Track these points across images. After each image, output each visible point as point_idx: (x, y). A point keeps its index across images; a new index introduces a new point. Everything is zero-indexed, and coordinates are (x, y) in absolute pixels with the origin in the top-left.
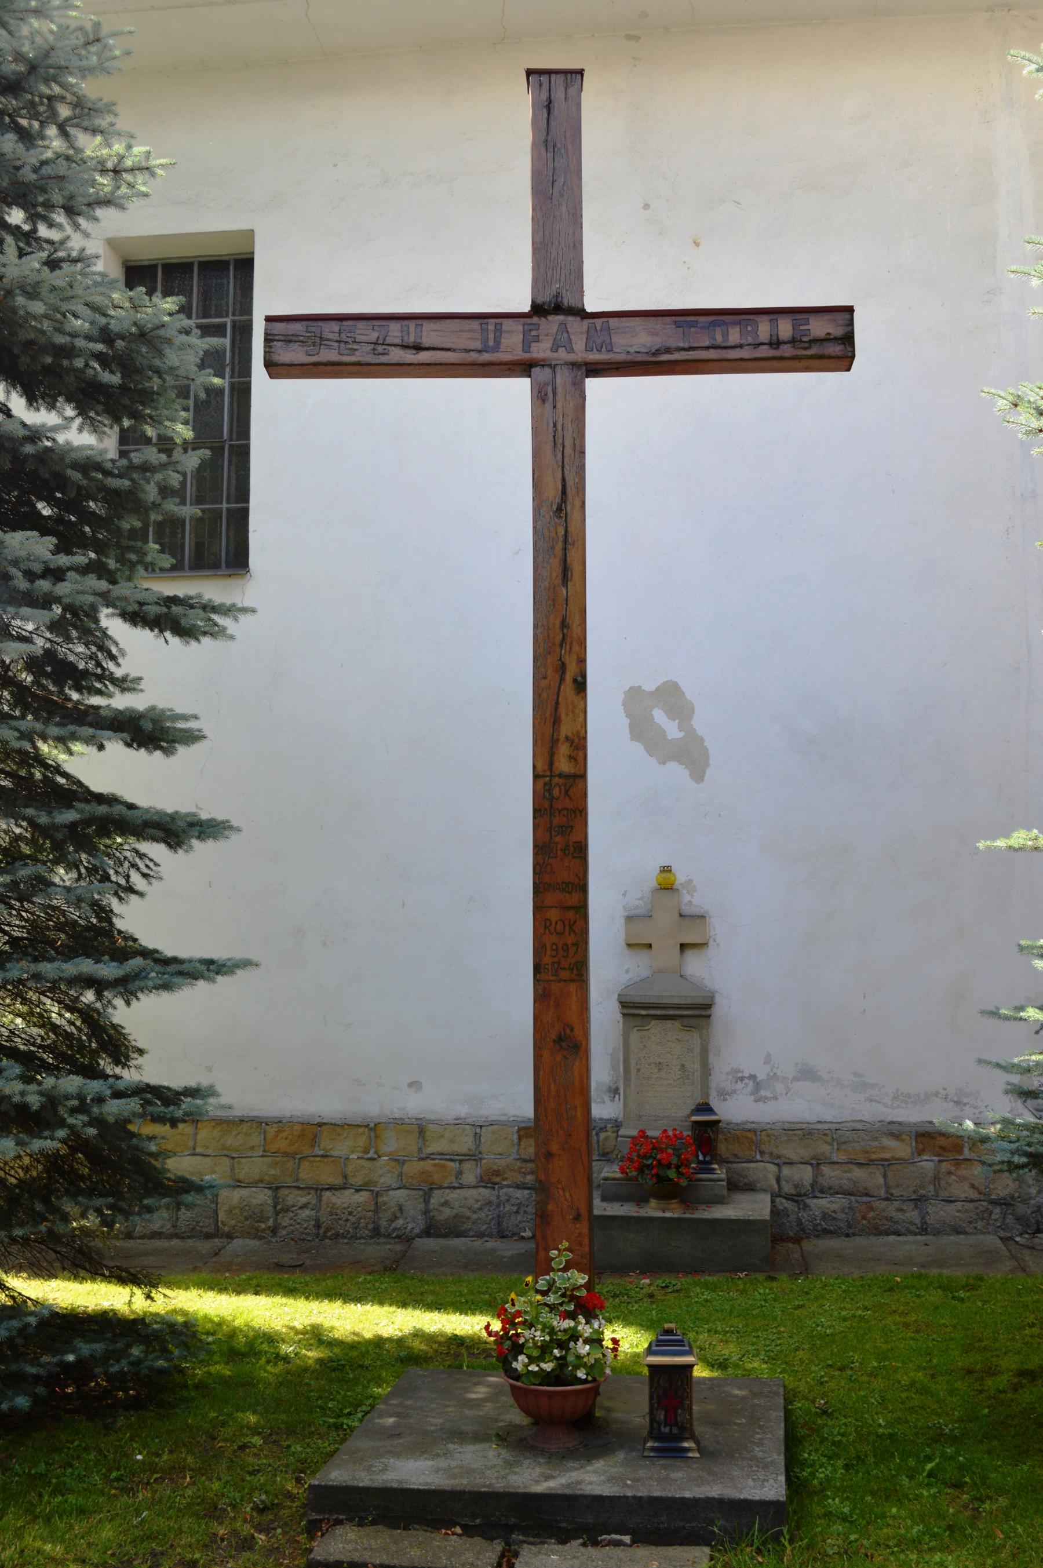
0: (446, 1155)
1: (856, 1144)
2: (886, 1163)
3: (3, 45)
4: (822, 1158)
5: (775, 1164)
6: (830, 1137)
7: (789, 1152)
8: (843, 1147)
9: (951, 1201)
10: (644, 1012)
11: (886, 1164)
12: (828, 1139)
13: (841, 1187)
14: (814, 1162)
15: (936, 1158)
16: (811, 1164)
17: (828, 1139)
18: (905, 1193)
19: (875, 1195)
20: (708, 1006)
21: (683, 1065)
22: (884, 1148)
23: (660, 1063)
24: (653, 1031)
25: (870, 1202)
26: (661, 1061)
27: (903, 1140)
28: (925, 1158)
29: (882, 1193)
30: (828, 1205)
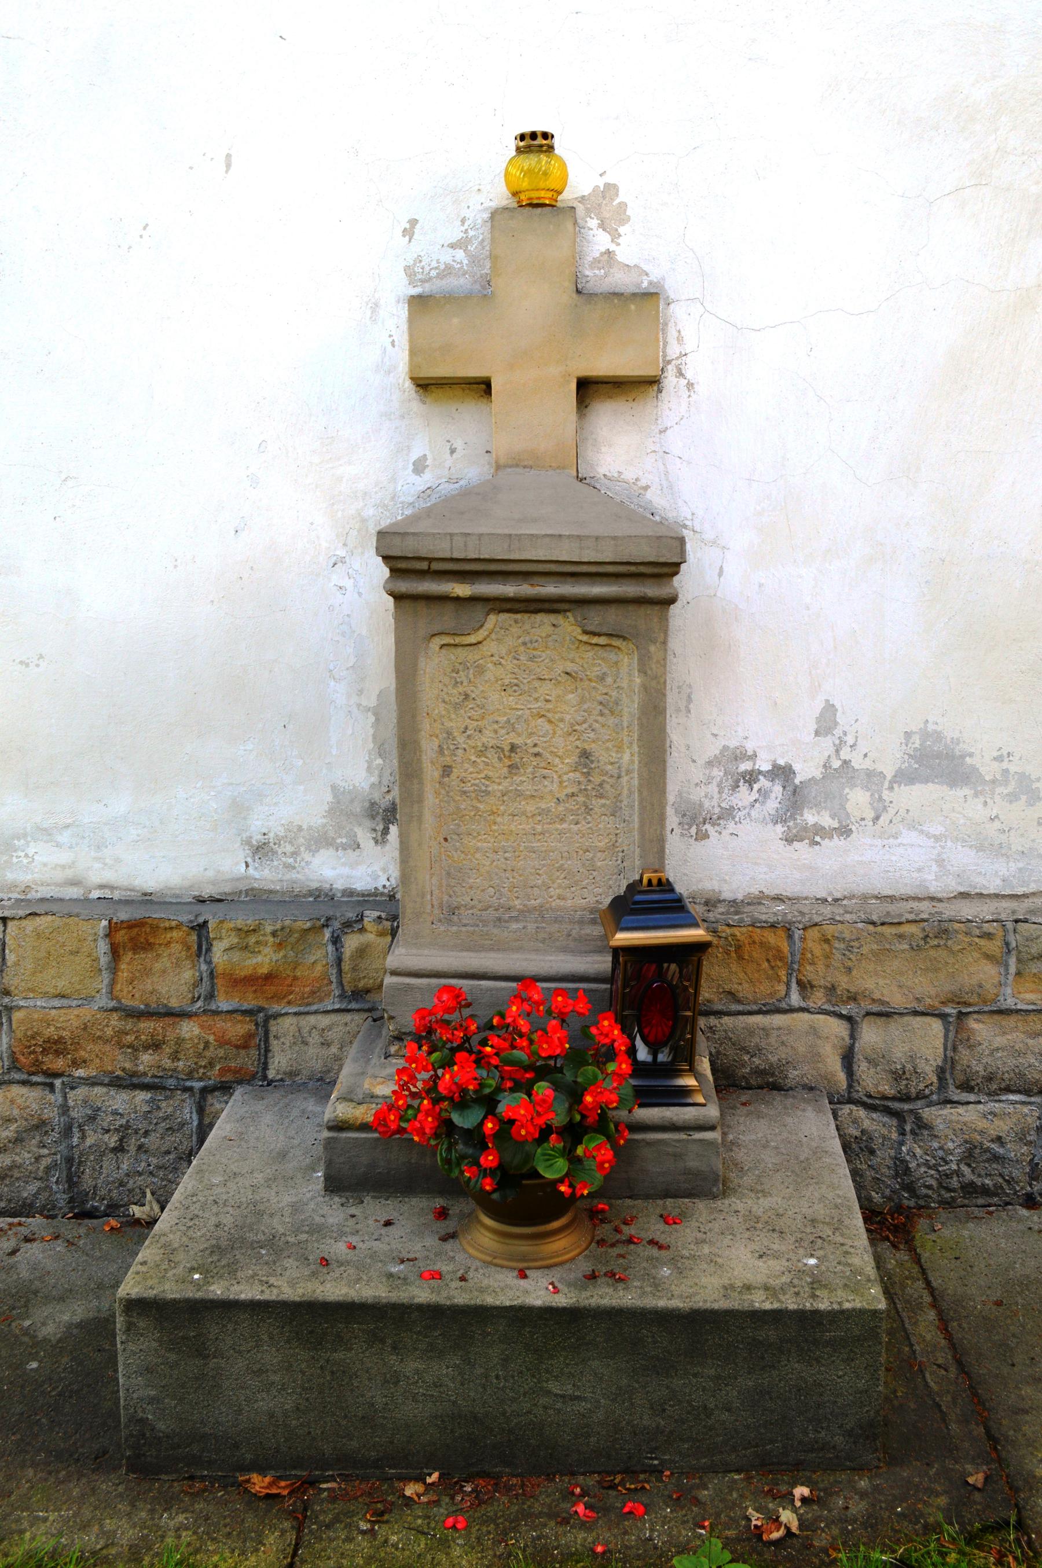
0: (473, 599)
4: (974, 999)
5: (840, 1016)
6: (998, 943)
10: (462, 590)
12: (994, 947)
16: (943, 1016)
20: (673, 568)
23: (513, 748)
26: (518, 741)
30: (982, 1124)
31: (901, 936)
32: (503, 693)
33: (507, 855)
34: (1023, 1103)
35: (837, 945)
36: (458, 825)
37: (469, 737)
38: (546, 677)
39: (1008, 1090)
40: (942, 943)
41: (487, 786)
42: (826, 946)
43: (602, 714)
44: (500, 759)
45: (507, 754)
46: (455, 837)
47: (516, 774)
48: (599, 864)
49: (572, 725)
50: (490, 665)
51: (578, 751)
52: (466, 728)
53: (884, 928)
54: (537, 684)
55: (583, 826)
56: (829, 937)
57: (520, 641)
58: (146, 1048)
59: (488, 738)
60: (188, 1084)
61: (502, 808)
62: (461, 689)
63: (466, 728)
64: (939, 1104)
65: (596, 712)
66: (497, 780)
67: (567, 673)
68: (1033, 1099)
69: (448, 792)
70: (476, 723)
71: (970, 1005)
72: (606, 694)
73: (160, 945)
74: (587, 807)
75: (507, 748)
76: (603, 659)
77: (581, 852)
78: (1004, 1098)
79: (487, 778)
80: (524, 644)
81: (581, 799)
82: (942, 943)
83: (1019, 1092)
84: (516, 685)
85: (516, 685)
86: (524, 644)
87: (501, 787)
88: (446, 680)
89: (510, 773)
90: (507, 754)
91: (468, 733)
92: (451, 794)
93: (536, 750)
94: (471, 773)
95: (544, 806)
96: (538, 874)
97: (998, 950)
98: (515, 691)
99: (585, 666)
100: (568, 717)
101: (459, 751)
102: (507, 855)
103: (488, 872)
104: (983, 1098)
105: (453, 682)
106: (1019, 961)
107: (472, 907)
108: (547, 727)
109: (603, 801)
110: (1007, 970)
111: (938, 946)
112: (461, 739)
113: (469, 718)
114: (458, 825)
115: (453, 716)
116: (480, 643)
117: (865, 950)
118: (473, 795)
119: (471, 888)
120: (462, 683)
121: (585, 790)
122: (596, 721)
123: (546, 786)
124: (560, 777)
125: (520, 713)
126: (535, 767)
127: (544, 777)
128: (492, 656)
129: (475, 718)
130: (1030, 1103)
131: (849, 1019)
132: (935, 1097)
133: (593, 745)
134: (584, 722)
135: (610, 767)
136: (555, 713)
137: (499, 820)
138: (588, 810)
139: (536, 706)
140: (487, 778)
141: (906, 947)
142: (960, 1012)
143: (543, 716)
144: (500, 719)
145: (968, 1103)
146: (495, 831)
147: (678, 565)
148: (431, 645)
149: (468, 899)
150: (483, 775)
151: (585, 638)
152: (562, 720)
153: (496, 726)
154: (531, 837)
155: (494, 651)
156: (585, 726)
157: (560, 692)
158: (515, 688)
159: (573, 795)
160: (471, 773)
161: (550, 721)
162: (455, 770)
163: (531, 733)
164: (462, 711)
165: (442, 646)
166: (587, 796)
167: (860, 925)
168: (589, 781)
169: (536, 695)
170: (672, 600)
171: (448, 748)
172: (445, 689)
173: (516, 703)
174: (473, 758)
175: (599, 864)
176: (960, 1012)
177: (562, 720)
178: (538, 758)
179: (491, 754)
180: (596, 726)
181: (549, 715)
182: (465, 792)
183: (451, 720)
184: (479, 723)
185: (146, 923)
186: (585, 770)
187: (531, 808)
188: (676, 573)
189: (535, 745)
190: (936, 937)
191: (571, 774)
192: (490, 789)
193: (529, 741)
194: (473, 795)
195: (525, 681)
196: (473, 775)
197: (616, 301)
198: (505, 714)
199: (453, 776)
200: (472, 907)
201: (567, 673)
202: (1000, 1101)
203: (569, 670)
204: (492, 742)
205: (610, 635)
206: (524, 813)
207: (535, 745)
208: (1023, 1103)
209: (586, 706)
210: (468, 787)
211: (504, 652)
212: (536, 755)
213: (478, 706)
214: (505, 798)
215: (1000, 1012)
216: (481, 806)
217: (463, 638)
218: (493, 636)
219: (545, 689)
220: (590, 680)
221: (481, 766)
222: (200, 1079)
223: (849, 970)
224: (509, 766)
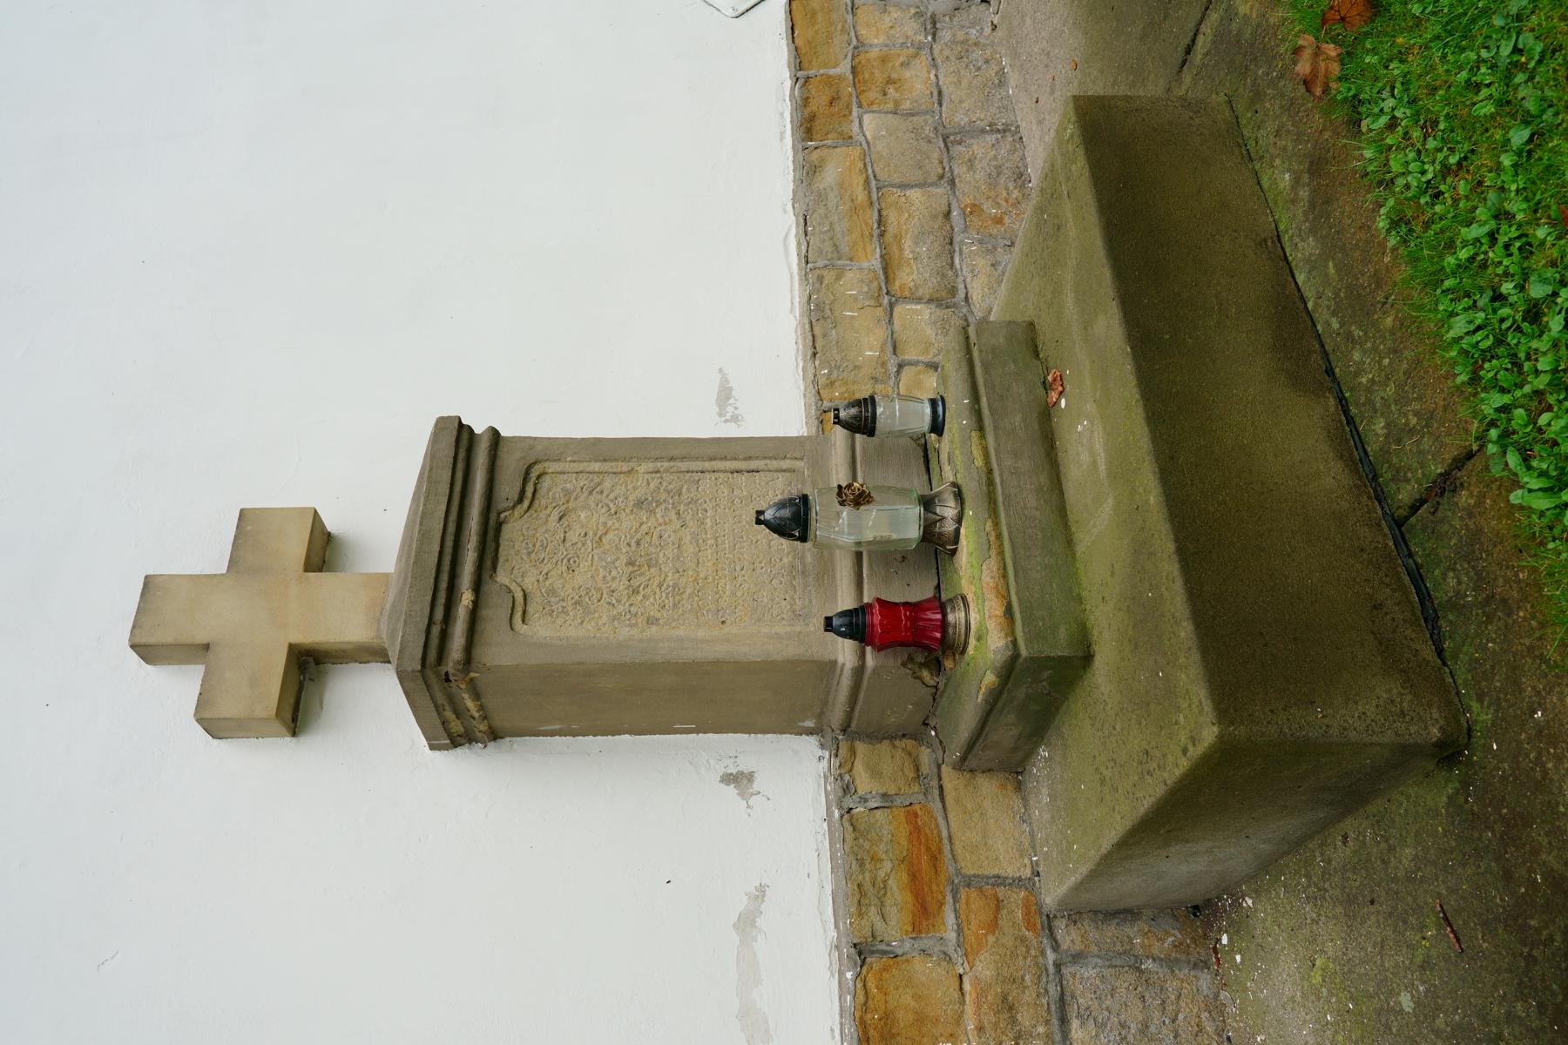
0: (477, 587)
1: (837, 228)
2: (873, 182)
3: (978, 1044)
4: (875, 285)
5: (898, 372)
6: (825, 273)
7: (869, 347)
8: (845, 249)
9: (940, 93)
10: (467, 598)
11: (876, 187)
12: (829, 276)
13: (938, 256)
14: (886, 301)
15: (855, 111)
16: (892, 306)
17: (829, 276)
18: (936, 155)
19: (944, 202)
20: (463, 434)
21: (639, 504)
22: (841, 185)
23: (630, 563)
24: (529, 583)
25: (963, 210)
26: (624, 559)
27: (822, 160)
28: (856, 128)
29: (941, 190)
30: (982, 279)
31: (825, 336)
32: (576, 572)
33: (738, 569)
34: (961, 254)
35: (835, 376)
36: (708, 611)
37: (619, 601)
38: (562, 535)
39: (952, 265)
40: (828, 307)
41: (668, 586)
42: (837, 384)
43: (602, 492)
44: (640, 575)
45: (636, 568)
46: (720, 614)
47: (657, 561)
48: (745, 493)
49: (611, 515)
50: (547, 583)
51: (635, 510)
52: (609, 603)
53: (817, 345)
54: (568, 544)
55: (709, 506)
56: (828, 382)
57: (525, 558)
58: (1013, 1021)
59: (621, 586)
60: (1051, 969)
61: (690, 573)
62: (570, 608)
63: (609, 603)
64: (969, 306)
65: (599, 497)
66: (663, 576)
67: (560, 519)
68: (957, 249)
69: (674, 620)
70: (605, 595)
71: (880, 288)
72: (582, 488)
73: (886, 1002)
74: (689, 503)
75: (631, 568)
76: (549, 490)
77: (734, 507)
78: (958, 267)
79: (660, 586)
80: (529, 554)
81: (682, 508)
82: (828, 307)
83: (952, 258)
84: (569, 561)
85: (569, 561)
86: (529, 554)
87: (670, 574)
88: (559, 621)
89: (655, 566)
90: (636, 568)
91: (614, 601)
92: (676, 617)
93: (633, 543)
94: (655, 600)
95: (689, 538)
96: (757, 542)
97: (832, 272)
98: (575, 562)
99: (554, 505)
100: (602, 519)
101: (632, 609)
102: (738, 569)
103: (756, 585)
104: (960, 279)
105: (562, 615)
106: (839, 259)
107: (792, 598)
108: (610, 536)
109: (684, 490)
110: (847, 265)
111: (831, 310)
112: (621, 608)
113: (599, 601)
114: (708, 611)
115: (596, 615)
116: (523, 590)
117: (838, 358)
118: (677, 598)
119: (772, 600)
120: (564, 607)
121: (673, 504)
122: (608, 496)
123: (669, 536)
124: (660, 525)
125: (596, 558)
126: (650, 545)
127: (661, 537)
128: (538, 581)
129: (599, 596)
130: (960, 249)
131: (900, 366)
132: (965, 310)
133: (631, 498)
134: (608, 505)
135: (652, 485)
136: (598, 529)
137: (702, 576)
138: (693, 501)
139: (590, 544)
140: (660, 586)
141: (834, 332)
142: (887, 294)
143: (600, 538)
144: (601, 576)
145: (966, 287)
146: (714, 579)
147: (461, 425)
148: (522, 632)
149: (784, 602)
150: (658, 589)
151: (526, 503)
152: (605, 523)
153: (609, 578)
154: (720, 547)
155: (534, 579)
156: (611, 505)
157: (578, 526)
158: (571, 562)
159: (678, 513)
160: (655, 600)
161: (606, 533)
162: (652, 614)
163: (617, 548)
164: (592, 607)
165: (523, 621)
166: (679, 503)
167: (817, 363)
168: (664, 501)
169: (579, 545)
170: (495, 434)
171: (629, 620)
172: (568, 623)
173: (586, 561)
174: (640, 598)
175: (745, 493)
176: (887, 294)
177: (605, 524)
178: (642, 542)
179: (635, 583)
180: (611, 496)
181: (600, 533)
182: (674, 605)
183: (601, 617)
184: (605, 592)
185: (861, 1018)
186: (654, 505)
187: (690, 549)
188: (470, 428)
189: (629, 545)
190: (823, 311)
191: (658, 516)
192: (671, 583)
193: (624, 550)
194: (677, 598)
195: (565, 553)
196: (657, 598)
197: (240, 541)
198: (597, 570)
199: (658, 615)
200: (792, 598)
201: (560, 519)
202: (961, 268)
203: (557, 518)
204: (624, 581)
205: (525, 480)
206: (696, 554)
207: (629, 545)
208: (961, 254)
209: (593, 505)
210: (670, 602)
211: (536, 572)
212: (638, 543)
213: (587, 593)
214: (681, 570)
215: (886, 270)
216: (689, 591)
217: (517, 603)
218: (519, 580)
219: (573, 537)
220: (568, 502)
221: (648, 590)
222: (1043, 953)
223: (856, 367)
224: (649, 566)
